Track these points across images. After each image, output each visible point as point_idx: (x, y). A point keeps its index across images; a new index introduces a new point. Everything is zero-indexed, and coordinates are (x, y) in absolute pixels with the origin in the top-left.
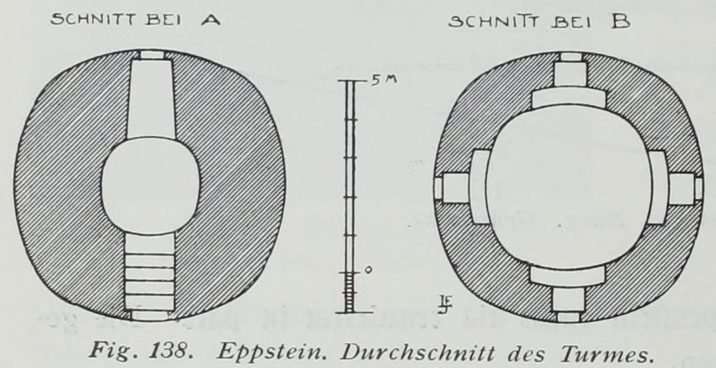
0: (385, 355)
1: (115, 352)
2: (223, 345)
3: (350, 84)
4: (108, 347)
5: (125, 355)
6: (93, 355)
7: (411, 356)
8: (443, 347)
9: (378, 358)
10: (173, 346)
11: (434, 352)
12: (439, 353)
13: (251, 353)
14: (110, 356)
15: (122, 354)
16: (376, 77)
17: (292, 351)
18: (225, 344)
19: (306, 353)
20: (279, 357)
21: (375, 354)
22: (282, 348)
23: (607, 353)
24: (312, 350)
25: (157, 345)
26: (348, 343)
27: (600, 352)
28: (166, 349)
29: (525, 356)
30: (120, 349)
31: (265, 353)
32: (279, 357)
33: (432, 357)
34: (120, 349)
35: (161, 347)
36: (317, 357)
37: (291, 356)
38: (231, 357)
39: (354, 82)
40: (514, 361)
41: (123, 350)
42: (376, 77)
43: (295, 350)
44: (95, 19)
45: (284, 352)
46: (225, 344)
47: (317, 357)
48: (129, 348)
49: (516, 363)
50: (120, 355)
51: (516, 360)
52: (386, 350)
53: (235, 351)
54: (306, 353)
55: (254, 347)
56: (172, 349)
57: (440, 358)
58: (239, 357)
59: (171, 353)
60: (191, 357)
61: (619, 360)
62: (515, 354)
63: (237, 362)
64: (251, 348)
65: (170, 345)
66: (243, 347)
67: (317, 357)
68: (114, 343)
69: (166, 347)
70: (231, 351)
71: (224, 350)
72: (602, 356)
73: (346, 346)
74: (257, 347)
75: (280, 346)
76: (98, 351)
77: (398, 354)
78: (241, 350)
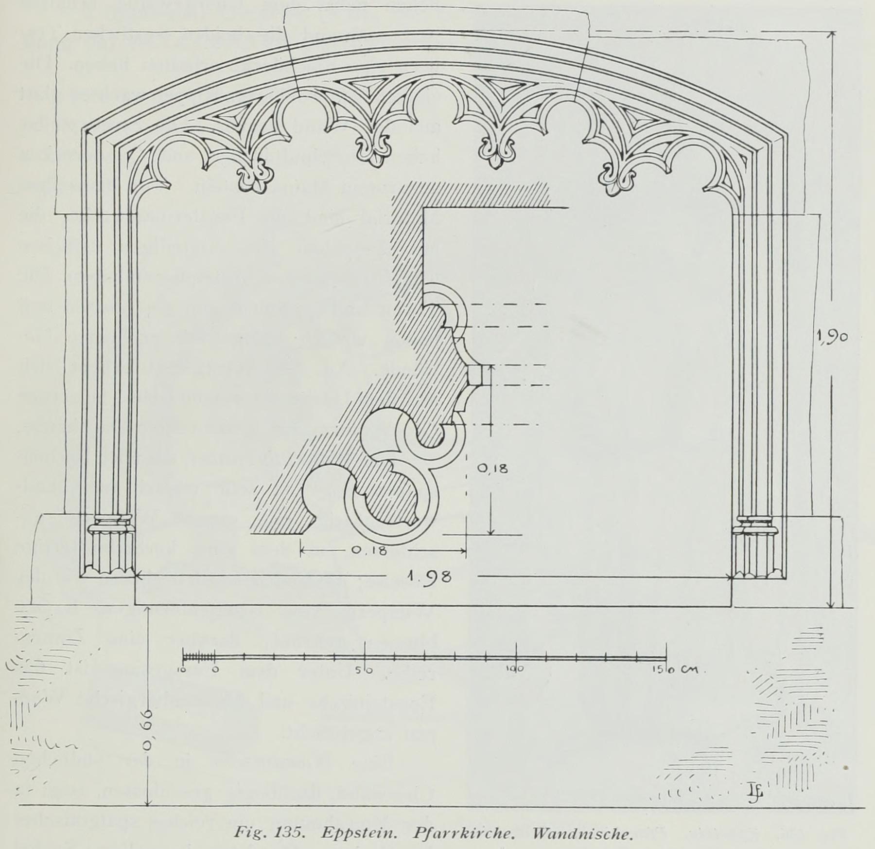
0: (483, 835)
1: (252, 834)
2: (325, 828)
3: (665, 659)
4: (247, 830)
5: (258, 835)
6: (237, 836)
7: (380, 835)
8: (495, 830)
9: (444, 836)
10: (291, 829)
11: (489, 833)
12: (611, 835)
13: (345, 834)
14: (248, 836)
15: (257, 835)
16: (358, 668)
17: (372, 833)
18: (240, 827)
19: (383, 834)
20: (364, 837)
21: (442, 835)
22: (366, 830)
23: (560, 832)
24: (386, 832)
25: (280, 829)
26: (536, 827)
27: (449, 832)
28: (286, 831)
29: (370, 834)
30: (255, 832)
31: (354, 834)
32: (364, 837)
33: (606, 837)
34: (255, 832)
35: (282, 831)
36: (390, 837)
37: (624, 838)
38: (331, 837)
39: (666, 661)
40: (437, 838)
41: (257, 832)
42: (358, 668)
43: (375, 831)
44: (142, 181)
45: (367, 833)
46: (240, 827)
47: (390, 837)
48: (261, 831)
49: (439, 839)
50: (255, 836)
51: (574, 838)
52: (483, 832)
53: (334, 833)
54: (383, 834)
55: (347, 830)
56: (290, 832)
57: (613, 838)
58: (336, 837)
59: (290, 835)
60: (304, 837)
61: (564, 838)
62: (573, 834)
63: (335, 840)
64: (345, 831)
65: (289, 829)
66: (339, 830)
67: (390, 837)
68: (251, 827)
69: (286, 830)
70: (331, 833)
71: (326, 832)
72: (451, 834)
73: (535, 829)
74: (349, 830)
75: (365, 829)
76: (240, 833)
77: (491, 835)
78: (338, 832)
